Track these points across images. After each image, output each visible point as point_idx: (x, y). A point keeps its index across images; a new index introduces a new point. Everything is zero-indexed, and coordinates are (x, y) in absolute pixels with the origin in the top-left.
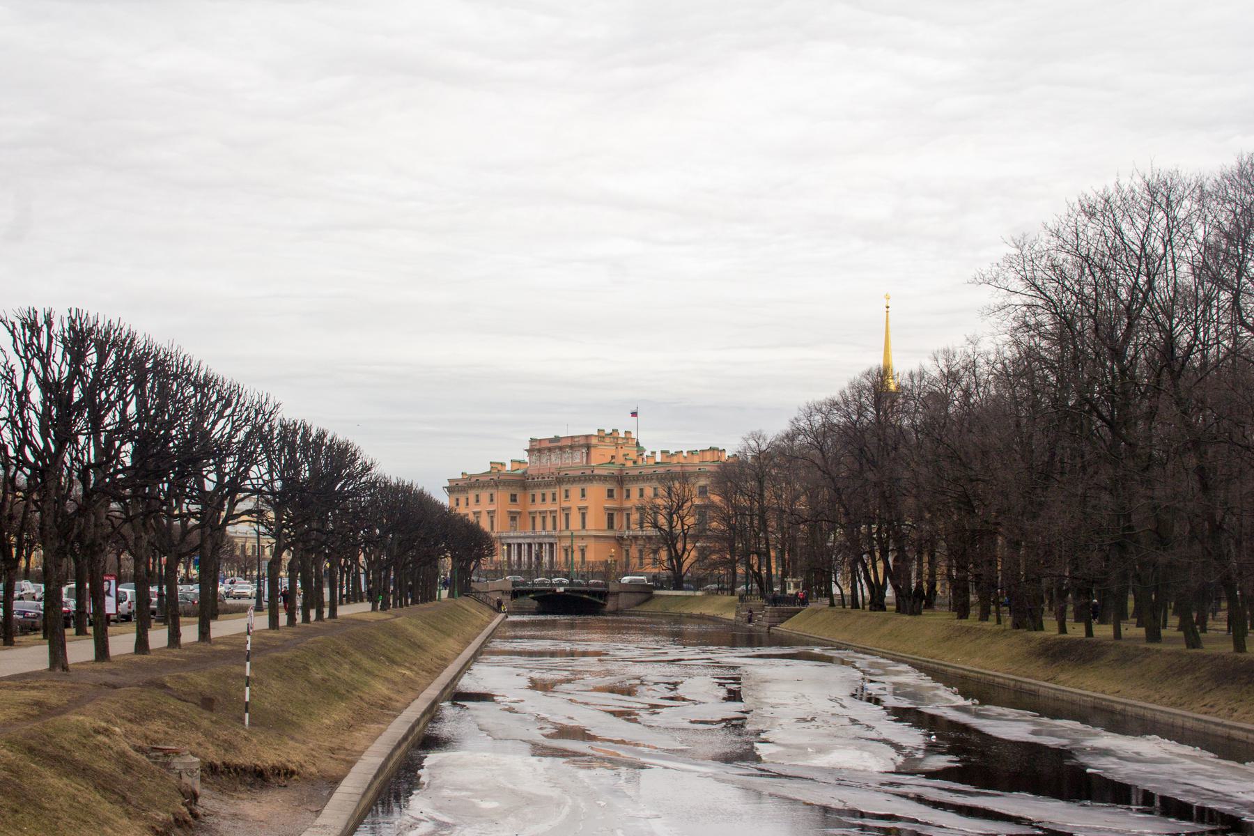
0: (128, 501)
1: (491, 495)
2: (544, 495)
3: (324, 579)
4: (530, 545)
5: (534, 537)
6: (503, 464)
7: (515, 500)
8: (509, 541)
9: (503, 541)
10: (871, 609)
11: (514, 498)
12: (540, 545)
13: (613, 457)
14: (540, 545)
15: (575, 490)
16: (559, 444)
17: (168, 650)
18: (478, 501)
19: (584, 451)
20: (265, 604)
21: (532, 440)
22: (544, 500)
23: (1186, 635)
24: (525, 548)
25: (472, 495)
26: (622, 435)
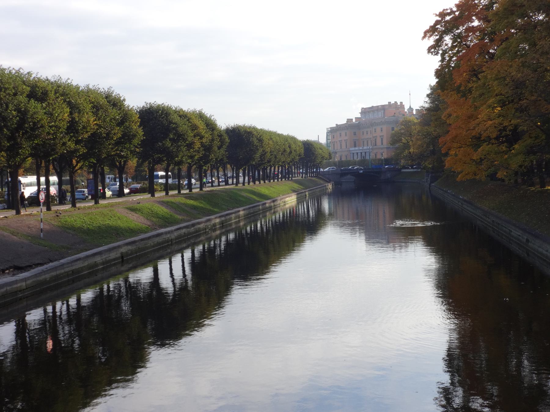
2: (367, 131)
4: (361, 153)
5: (363, 150)
6: (352, 120)
7: (356, 134)
8: (353, 152)
9: (351, 152)
11: (355, 134)
12: (365, 153)
13: (395, 113)
14: (365, 153)
15: (378, 128)
16: (372, 109)
17: (16, 216)
18: (340, 136)
20: (343, 172)
21: (347, 119)
22: (367, 134)
24: (359, 154)
25: (338, 133)
26: (399, 104)
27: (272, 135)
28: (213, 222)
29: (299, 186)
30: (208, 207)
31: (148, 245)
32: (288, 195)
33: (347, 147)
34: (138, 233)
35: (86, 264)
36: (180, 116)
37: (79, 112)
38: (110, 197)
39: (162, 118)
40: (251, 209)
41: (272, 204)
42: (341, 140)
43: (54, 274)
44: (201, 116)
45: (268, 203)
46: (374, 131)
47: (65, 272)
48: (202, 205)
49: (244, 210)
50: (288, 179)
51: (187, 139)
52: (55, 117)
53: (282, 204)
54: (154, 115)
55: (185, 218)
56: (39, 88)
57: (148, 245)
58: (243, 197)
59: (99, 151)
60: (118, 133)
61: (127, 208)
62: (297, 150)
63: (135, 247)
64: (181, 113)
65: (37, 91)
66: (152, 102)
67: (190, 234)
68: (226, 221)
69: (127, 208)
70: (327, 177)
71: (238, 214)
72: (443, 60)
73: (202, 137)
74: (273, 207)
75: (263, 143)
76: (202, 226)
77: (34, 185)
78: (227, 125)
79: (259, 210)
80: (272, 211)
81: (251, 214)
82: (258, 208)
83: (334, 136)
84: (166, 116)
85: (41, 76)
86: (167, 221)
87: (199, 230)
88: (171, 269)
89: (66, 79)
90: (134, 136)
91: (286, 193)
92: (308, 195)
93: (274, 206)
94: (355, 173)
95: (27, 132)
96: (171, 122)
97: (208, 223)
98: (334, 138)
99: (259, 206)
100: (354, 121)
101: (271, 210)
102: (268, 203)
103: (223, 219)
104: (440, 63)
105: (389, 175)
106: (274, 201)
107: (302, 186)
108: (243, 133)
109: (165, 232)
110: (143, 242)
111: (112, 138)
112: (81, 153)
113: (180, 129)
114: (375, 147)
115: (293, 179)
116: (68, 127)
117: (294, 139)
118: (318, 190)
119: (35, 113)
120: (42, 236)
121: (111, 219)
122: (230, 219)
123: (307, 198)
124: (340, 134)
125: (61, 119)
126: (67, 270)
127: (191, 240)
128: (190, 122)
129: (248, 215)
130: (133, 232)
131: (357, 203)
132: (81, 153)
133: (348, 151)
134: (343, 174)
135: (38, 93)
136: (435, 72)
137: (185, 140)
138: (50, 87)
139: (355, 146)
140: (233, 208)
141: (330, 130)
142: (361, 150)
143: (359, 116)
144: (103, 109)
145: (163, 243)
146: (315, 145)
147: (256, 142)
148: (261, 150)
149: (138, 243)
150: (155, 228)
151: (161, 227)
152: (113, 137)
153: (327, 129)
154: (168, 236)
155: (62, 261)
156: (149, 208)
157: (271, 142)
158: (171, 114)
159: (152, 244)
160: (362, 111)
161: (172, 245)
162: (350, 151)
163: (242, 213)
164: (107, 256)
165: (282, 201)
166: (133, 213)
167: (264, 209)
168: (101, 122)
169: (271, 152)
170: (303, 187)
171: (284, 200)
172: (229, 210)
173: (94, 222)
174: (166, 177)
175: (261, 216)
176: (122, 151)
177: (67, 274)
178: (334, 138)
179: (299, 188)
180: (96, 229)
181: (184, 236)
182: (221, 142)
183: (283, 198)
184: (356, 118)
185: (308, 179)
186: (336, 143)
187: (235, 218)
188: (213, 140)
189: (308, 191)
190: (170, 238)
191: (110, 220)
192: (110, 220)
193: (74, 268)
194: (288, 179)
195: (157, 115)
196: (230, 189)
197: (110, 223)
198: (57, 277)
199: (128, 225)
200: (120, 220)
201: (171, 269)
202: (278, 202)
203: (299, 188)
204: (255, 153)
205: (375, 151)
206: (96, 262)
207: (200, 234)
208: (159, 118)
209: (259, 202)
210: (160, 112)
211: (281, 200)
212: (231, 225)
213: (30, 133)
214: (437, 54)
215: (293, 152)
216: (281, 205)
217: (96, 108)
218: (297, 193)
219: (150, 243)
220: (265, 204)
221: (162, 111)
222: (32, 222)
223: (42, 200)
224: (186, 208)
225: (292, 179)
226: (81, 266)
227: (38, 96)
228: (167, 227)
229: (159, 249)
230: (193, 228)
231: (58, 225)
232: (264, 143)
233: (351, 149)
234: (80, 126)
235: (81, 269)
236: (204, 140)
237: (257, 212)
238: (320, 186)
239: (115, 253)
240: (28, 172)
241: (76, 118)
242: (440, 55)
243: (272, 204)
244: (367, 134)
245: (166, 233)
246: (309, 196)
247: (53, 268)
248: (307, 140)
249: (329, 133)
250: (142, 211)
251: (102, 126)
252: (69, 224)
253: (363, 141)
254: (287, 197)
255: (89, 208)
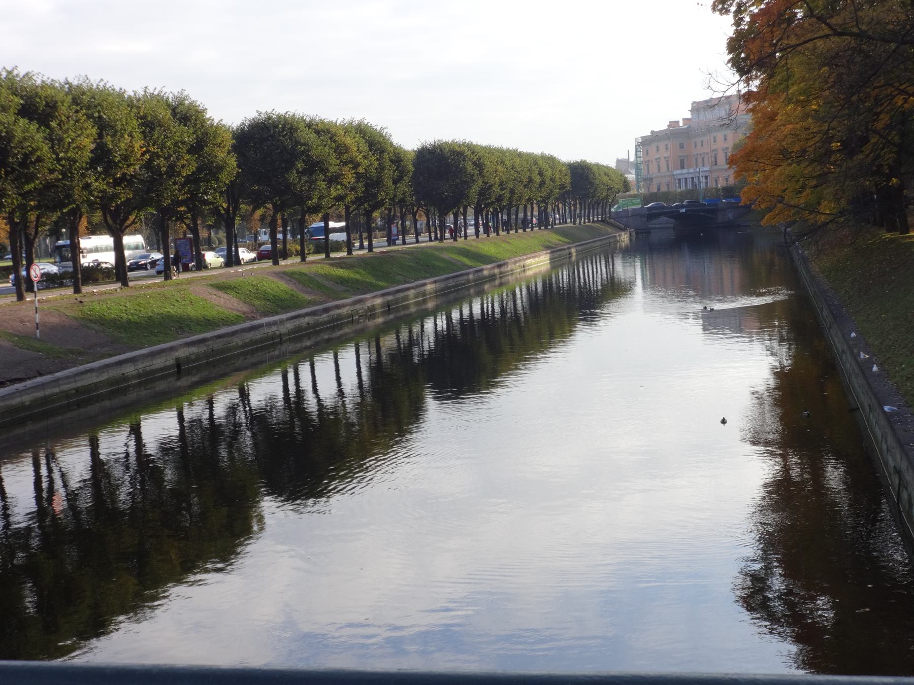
0: (800, 252)
1: (666, 145)
3: (555, 291)
4: (693, 179)
6: (678, 122)
7: (683, 148)
8: (680, 177)
10: (151, 268)
11: (682, 146)
18: (658, 150)
19: (727, 107)
21: (670, 122)
22: (702, 145)
23: (17, 288)
24: (689, 181)
25: (654, 146)
27: (502, 156)
28: (369, 304)
29: (562, 239)
30: (370, 279)
31: (231, 345)
32: (531, 256)
33: (668, 170)
34: (219, 326)
35: (104, 377)
36: (318, 132)
37: (114, 136)
38: (221, 266)
39: (284, 136)
40: (451, 280)
41: (496, 271)
42: (659, 158)
43: (40, 394)
44: (362, 131)
45: (487, 270)
46: (712, 141)
47: (62, 392)
48: (358, 277)
49: (432, 283)
50: (546, 228)
51: (327, 169)
52: (66, 144)
53: (518, 270)
54: (270, 131)
55: (318, 298)
56: (40, 98)
57: (231, 345)
58: (443, 260)
59: (157, 196)
60: (189, 165)
61: (212, 286)
62: (557, 179)
63: (205, 348)
64: (321, 126)
65: (38, 103)
66: (270, 111)
67: (317, 324)
68: (397, 301)
69: (212, 286)
70: (620, 222)
71: (422, 289)
72: (738, 23)
73: (356, 165)
74: (498, 276)
75: (484, 169)
76: (344, 311)
77: (110, 250)
78: (423, 141)
79: (468, 281)
80: (497, 282)
81: (448, 289)
82: (466, 278)
83: (647, 150)
84: (291, 132)
85: (48, 78)
86: (280, 304)
87: (340, 317)
88: (338, 378)
89: (97, 81)
90: (220, 168)
91: (532, 251)
92: (574, 254)
93: (501, 273)
94: (674, 214)
95: (14, 170)
96: (297, 143)
97: (358, 306)
98: (647, 154)
99: (468, 274)
100: (681, 124)
101: (495, 279)
102: (486, 269)
103: (390, 298)
104: (734, 28)
105: (730, 215)
106: (500, 266)
107: (567, 238)
108: (449, 154)
109: (266, 323)
110: (220, 340)
111: (179, 174)
112: (123, 199)
113: (314, 154)
114: (716, 167)
115: (555, 227)
116: (91, 159)
117: (551, 161)
118: (599, 243)
119: (25, 139)
120: (38, 335)
121: (176, 304)
122: (406, 298)
123: (574, 258)
124: (657, 147)
125: (77, 147)
126: (65, 387)
127: (322, 335)
128: (334, 141)
129: (442, 290)
130: (209, 323)
131: (686, 263)
132: (123, 199)
133: (670, 176)
134: (652, 215)
135: (40, 106)
136: (727, 43)
137: (324, 171)
138: (60, 97)
139: (682, 167)
140: (418, 279)
141: (640, 141)
142: (692, 173)
143: (689, 115)
144: (160, 126)
145: (261, 340)
146: (595, 169)
147: (469, 167)
148: (480, 182)
149: (210, 343)
150: (254, 317)
151: (266, 314)
152: (180, 172)
153: (636, 139)
154: (274, 328)
155: (58, 374)
156: (252, 285)
157: (500, 168)
158: (299, 129)
159: (240, 343)
160: (692, 107)
161: (281, 343)
162: (673, 175)
163: (430, 287)
164: (146, 364)
165: (517, 265)
166: (221, 294)
167: (478, 280)
168: (157, 148)
169: (501, 184)
170: (569, 241)
171: (522, 263)
172: (406, 282)
173: (142, 309)
174: (327, 231)
175: (472, 291)
176: (206, 194)
177: (66, 395)
178: (647, 154)
179: (561, 242)
180: (142, 321)
181: (306, 329)
182: (400, 171)
183: (520, 261)
184: (684, 119)
185: (588, 226)
186: (650, 162)
187: (416, 296)
188: (381, 168)
189: (576, 246)
190: (278, 333)
191: (174, 305)
192: (174, 305)
193: (79, 384)
194: (546, 228)
195: (275, 132)
196: (424, 248)
197: (171, 311)
198: (46, 400)
199: (205, 313)
200: (193, 305)
201: (338, 378)
202: (509, 266)
203: (561, 242)
204: (470, 188)
205: (715, 175)
206: (123, 374)
207: (342, 324)
208: (279, 136)
209: (471, 267)
210: (280, 126)
211: (515, 263)
212: (407, 307)
213: (18, 171)
214: (727, 11)
215: (548, 181)
216: (515, 271)
217: (149, 125)
218: (552, 250)
219: (237, 341)
220: (482, 270)
221: (284, 126)
222: (99, 308)
223: (36, 277)
224: (326, 283)
225: (552, 227)
226: (94, 381)
227: (39, 111)
228: (277, 313)
229: (257, 350)
230: (325, 315)
231: (76, 316)
232: (486, 170)
233: (675, 172)
234: (115, 157)
235: (96, 386)
236: (361, 170)
237: (463, 284)
238: (604, 237)
239: (165, 358)
240: (93, 230)
241: (108, 143)
242: (731, 15)
243: (496, 271)
244: (702, 145)
245: (269, 325)
246: (577, 255)
247: (39, 385)
248: (581, 161)
249: (639, 145)
250: (239, 290)
251: (160, 153)
252: (96, 315)
253: (648, 165)
254: (530, 258)
255: (158, 285)
